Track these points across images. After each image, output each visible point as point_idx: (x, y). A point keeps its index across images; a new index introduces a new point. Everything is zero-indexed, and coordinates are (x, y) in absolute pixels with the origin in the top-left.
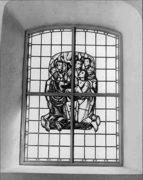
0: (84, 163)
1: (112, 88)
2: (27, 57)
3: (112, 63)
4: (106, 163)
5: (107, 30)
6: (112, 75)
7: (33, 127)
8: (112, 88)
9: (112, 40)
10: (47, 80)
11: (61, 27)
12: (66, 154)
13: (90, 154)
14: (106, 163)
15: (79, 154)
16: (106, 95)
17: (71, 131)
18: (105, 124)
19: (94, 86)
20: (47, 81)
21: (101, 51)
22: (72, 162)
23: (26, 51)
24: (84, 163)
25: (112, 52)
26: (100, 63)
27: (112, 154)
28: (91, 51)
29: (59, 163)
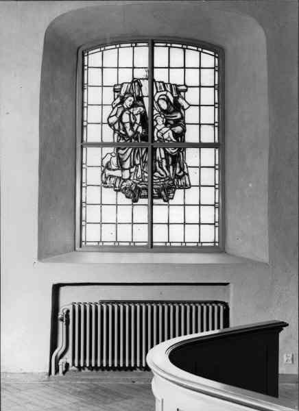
1: (209, 135)
15: (160, 236)
21: (192, 78)
25: (209, 77)
26: (192, 96)
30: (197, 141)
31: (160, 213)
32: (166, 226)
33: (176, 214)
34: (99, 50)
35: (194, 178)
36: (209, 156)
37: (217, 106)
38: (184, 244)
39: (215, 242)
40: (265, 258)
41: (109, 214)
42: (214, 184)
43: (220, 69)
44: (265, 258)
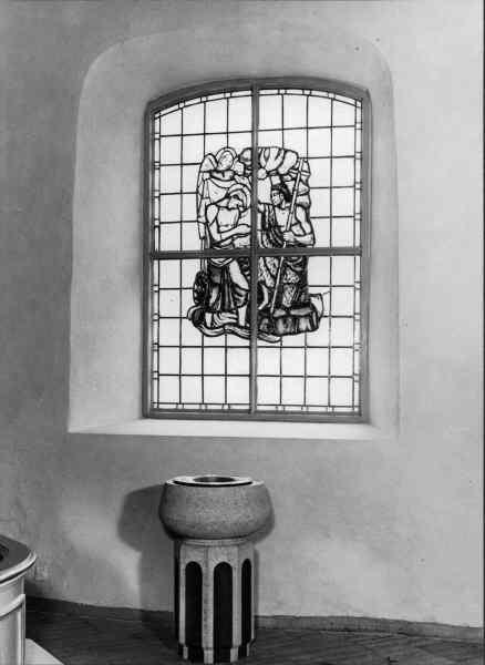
0: (279, 415)
1: (345, 234)
2: (149, 166)
3: (347, 172)
4: (330, 417)
5: (333, 88)
6: (347, 202)
7: (167, 332)
8: (345, 234)
9: (346, 112)
10: (200, 334)
11: (227, 86)
12: (238, 394)
13: (293, 396)
14: (330, 417)
15: (268, 395)
16: (330, 252)
17: (256, 610)
18: (333, 240)
19: (305, 168)
20: (204, 334)
21: (319, 143)
22: (251, 414)
23: (207, 595)
24: (279, 415)
25: (347, 141)
26: (319, 173)
27: (344, 395)
28: (295, 141)
29: (227, 414)
30: (327, 245)
31: (268, 359)
32: (179, 167)
33: (293, 361)
34: (198, 100)
35: (191, 174)
36: (346, 268)
37: (157, 136)
38: (157, 136)
39: (353, 406)
40: (313, 299)
41: (191, 361)
42: (352, 314)
43: (366, 127)
44: (313, 299)
